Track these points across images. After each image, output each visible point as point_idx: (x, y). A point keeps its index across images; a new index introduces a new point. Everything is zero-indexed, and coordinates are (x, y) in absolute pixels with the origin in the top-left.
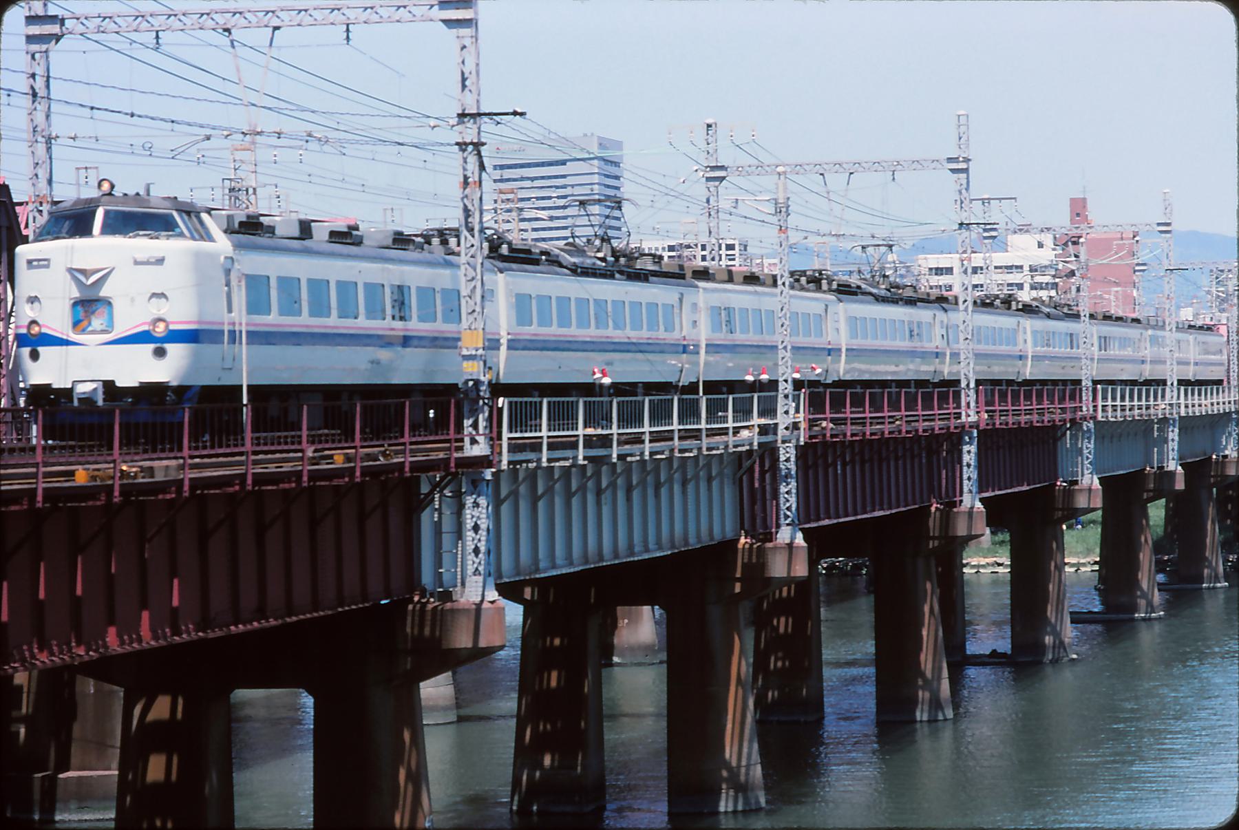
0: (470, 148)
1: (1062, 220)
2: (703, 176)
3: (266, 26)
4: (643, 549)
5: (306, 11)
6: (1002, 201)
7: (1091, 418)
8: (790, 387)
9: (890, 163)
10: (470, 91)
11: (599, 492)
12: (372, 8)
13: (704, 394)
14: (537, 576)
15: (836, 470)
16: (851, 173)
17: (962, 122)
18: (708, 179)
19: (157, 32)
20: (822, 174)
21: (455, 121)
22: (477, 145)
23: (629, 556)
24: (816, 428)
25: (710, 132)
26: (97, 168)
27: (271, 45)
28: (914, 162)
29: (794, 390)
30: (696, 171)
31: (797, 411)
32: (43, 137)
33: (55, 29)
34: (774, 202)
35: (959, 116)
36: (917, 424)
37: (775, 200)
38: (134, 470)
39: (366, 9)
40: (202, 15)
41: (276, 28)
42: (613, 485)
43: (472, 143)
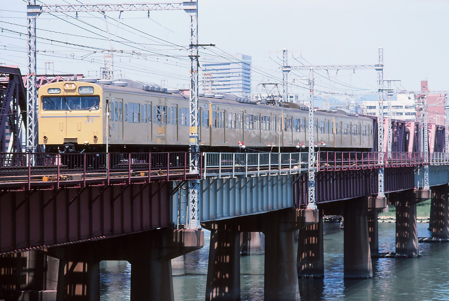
0: (194, 58)
1: (418, 89)
2: (282, 70)
3: (118, 10)
4: (256, 210)
6: (395, 81)
7: (427, 164)
8: (313, 150)
9: (353, 66)
10: (194, 36)
11: (240, 189)
12: (158, 4)
13: (280, 152)
14: (216, 220)
15: (330, 182)
16: (338, 70)
17: (381, 51)
18: (284, 71)
19: (77, 12)
22: (197, 57)
23: (250, 213)
24: (322, 166)
25: (284, 53)
26: (53, 63)
27: (119, 18)
29: (315, 151)
30: (279, 68)
31: (316, 159)
33: (38, 10)
35: (379, 49)
37: (309, 79)
38: (65, 177)
39: (156, 4)
40: (94, 6)
41: (122, 11)
43: (194, 56)
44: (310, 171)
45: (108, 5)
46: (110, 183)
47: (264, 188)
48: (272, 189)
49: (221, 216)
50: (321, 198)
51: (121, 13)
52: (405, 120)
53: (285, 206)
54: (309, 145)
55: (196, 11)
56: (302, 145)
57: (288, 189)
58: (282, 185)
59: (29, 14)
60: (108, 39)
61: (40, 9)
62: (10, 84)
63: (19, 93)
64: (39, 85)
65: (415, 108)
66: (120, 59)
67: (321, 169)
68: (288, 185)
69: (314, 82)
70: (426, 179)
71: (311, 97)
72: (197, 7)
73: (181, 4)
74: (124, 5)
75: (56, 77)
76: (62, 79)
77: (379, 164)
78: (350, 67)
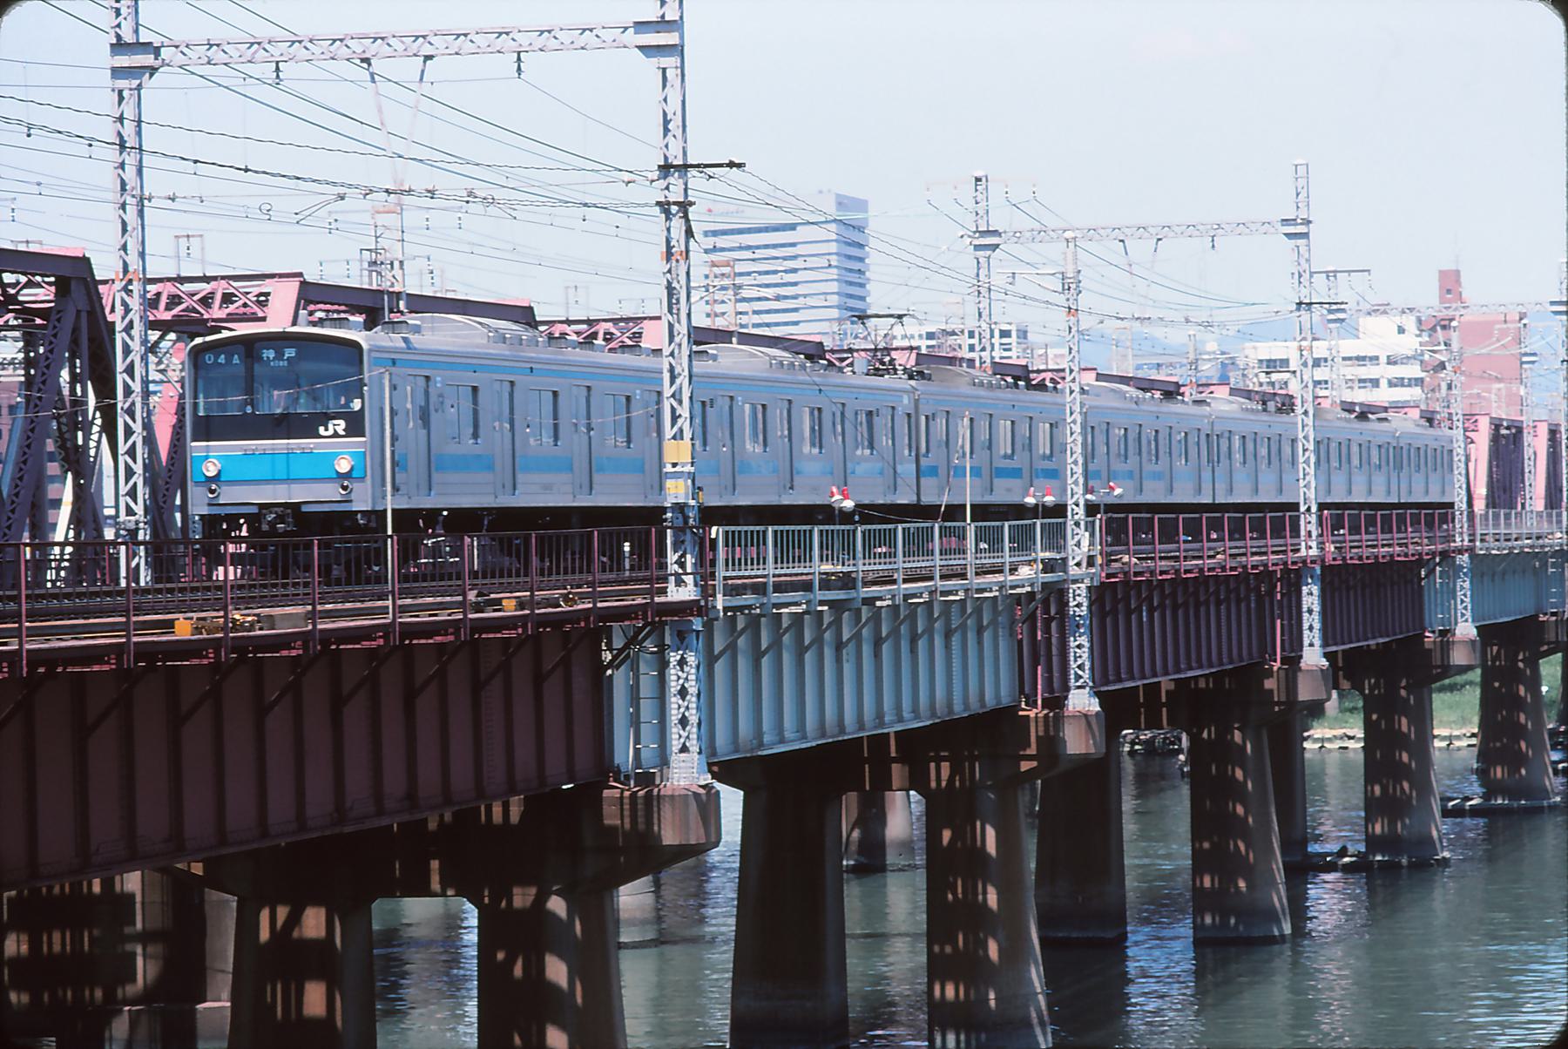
0: (674, 209)
1: (1429, 300)
2: (971, 244)
3: (415, 55)
5: (465, 35)
6: (1352, 274)
8: (1081, 511)
9: (1209, 227)
10: (674, 136)
11: (839, 646)
12: (549, 32)
13: (972, 521)
14: (760, 753)
17: (1302, 173)
19: (277, 63)
20: (1122, 241)
21: (656, 175)
23: (876, 728)
26: (201, 236)
27: (421, 79)
28: (1114, 229)
30: (962, 237)
32: (133, 196)
33: (148, 60)
34: (1061, 276)
35: (1296, 166)
36: (1244, 559)
38: (250, 619)
40: (335, 41)
41: (428, 58)
42: (857, 637)
43: (675, 203)
44: (1075, 581)
45: (383, 39)
46: (403, 636)
47: (920, 642)
48: (948, 646)
49: (777, 738)
50: (1404, 626)
51: (425, 62)
52: (1390, 402)
53: (990, 702)
54: (1069, 496)
55: (677, 50)
56: (1044, 496)
57: (1001, 643)
58: (980, 631)
59: (117, 72)
60: (384, 153)
61: (152, 56)
62: (59, 312)
63: (90, 340)
64: (154, 311)
65: (1422, 362)
66: (427, 219)
67: (1109, 576)
68: (1000, 630)
69: (1080, 282)
70: (1462, 601)
71: (1070, 332)
72: (682, 37)
73: (626, 28)
74: (436, 35)
75: (213, 284)
76: (232, 290)
77: (1303, 552)
78: (1201, 227)
